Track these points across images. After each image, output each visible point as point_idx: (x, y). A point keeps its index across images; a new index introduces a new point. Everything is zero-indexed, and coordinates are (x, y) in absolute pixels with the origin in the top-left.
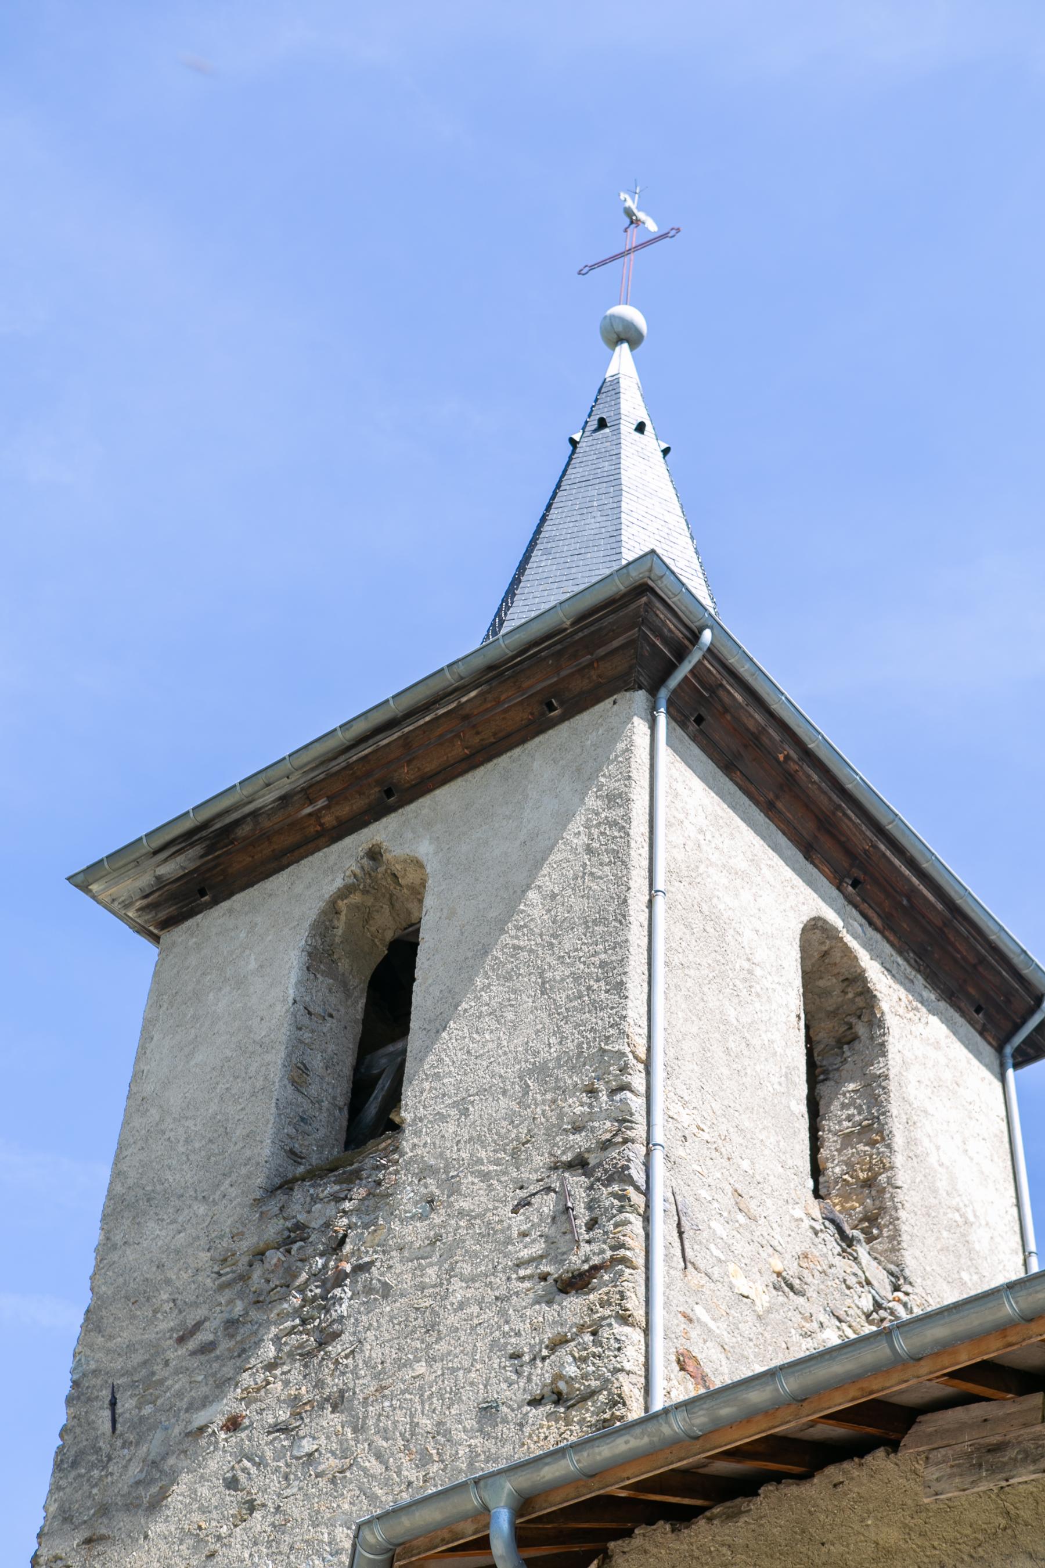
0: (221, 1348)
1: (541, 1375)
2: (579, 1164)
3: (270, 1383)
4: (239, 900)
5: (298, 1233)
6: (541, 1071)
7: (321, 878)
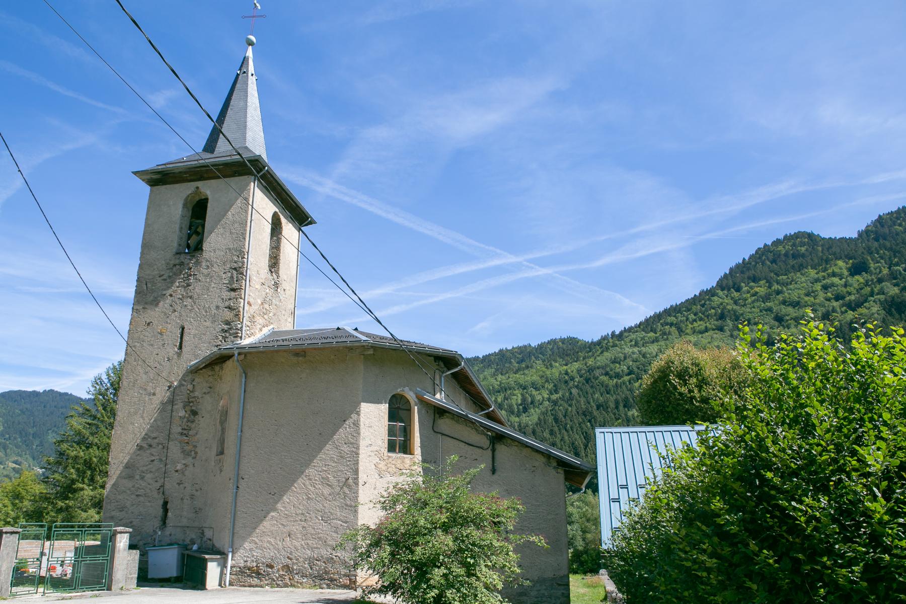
0: (169, 281)
1: (227, 304)
2: (235, 269)
3: (176, 288)
4: (168, 186)
5: (182, 264)
6: (229, 249)
7: (185, 190)
